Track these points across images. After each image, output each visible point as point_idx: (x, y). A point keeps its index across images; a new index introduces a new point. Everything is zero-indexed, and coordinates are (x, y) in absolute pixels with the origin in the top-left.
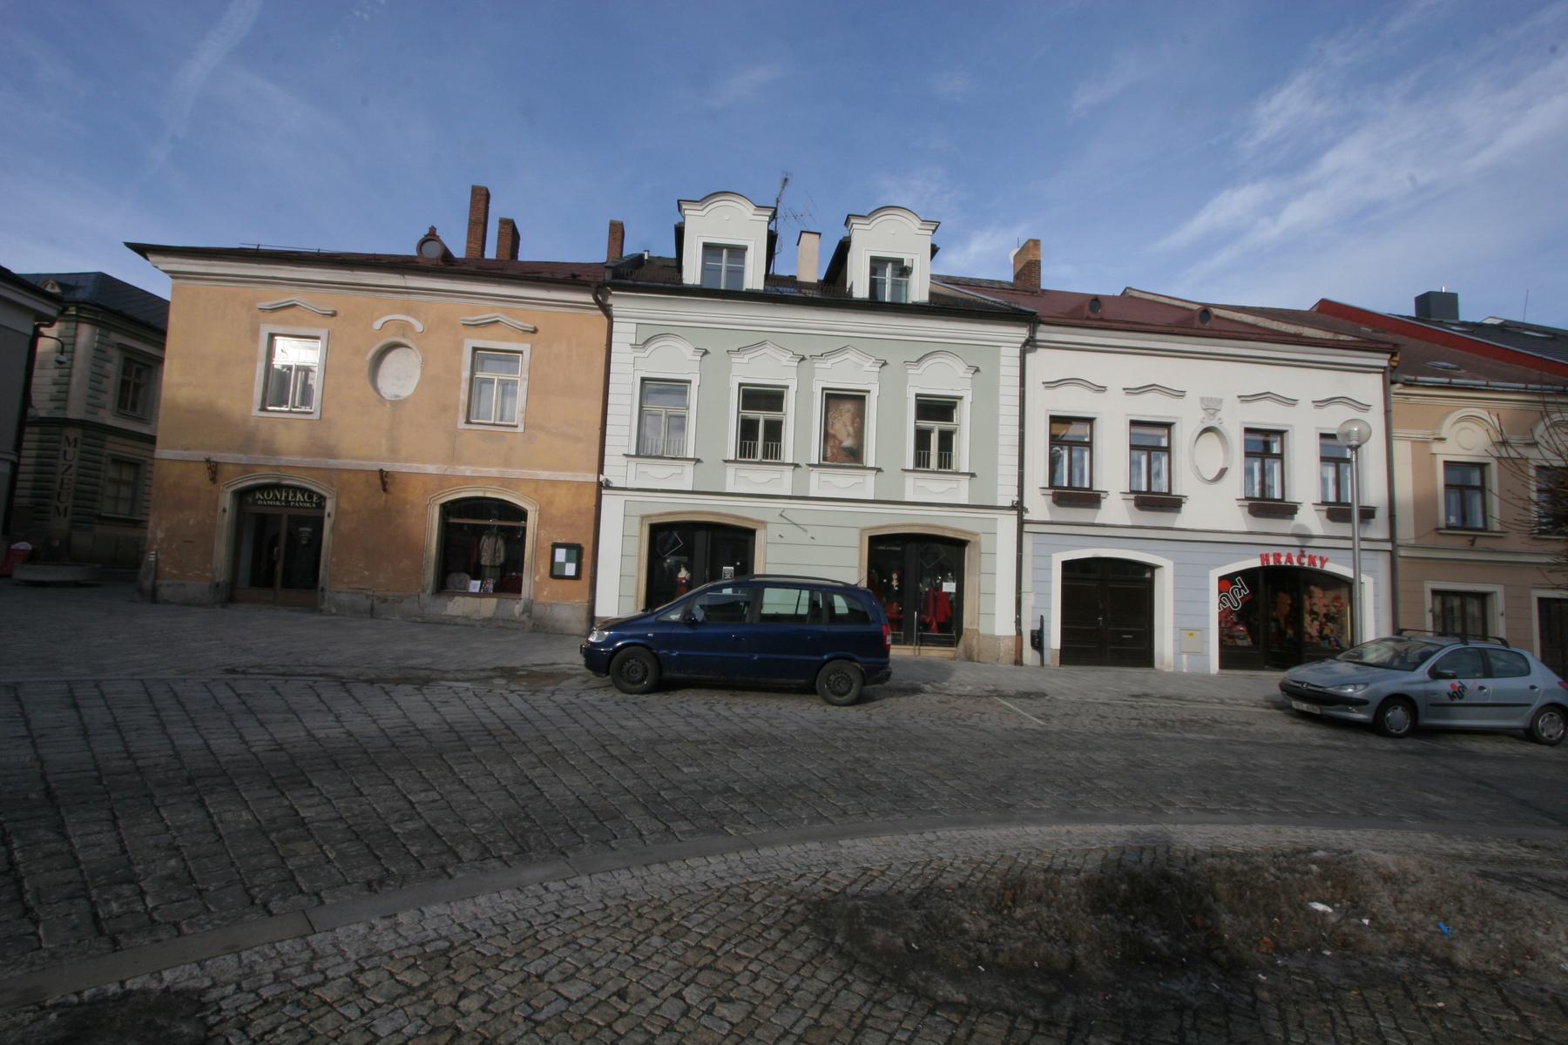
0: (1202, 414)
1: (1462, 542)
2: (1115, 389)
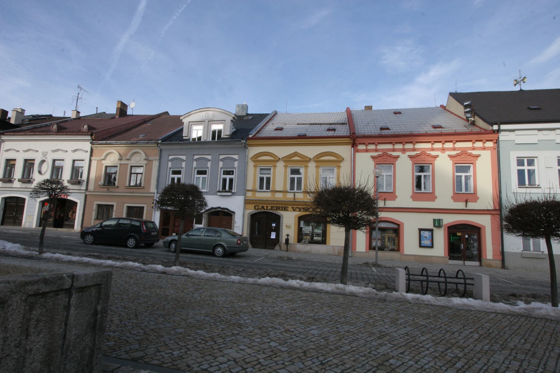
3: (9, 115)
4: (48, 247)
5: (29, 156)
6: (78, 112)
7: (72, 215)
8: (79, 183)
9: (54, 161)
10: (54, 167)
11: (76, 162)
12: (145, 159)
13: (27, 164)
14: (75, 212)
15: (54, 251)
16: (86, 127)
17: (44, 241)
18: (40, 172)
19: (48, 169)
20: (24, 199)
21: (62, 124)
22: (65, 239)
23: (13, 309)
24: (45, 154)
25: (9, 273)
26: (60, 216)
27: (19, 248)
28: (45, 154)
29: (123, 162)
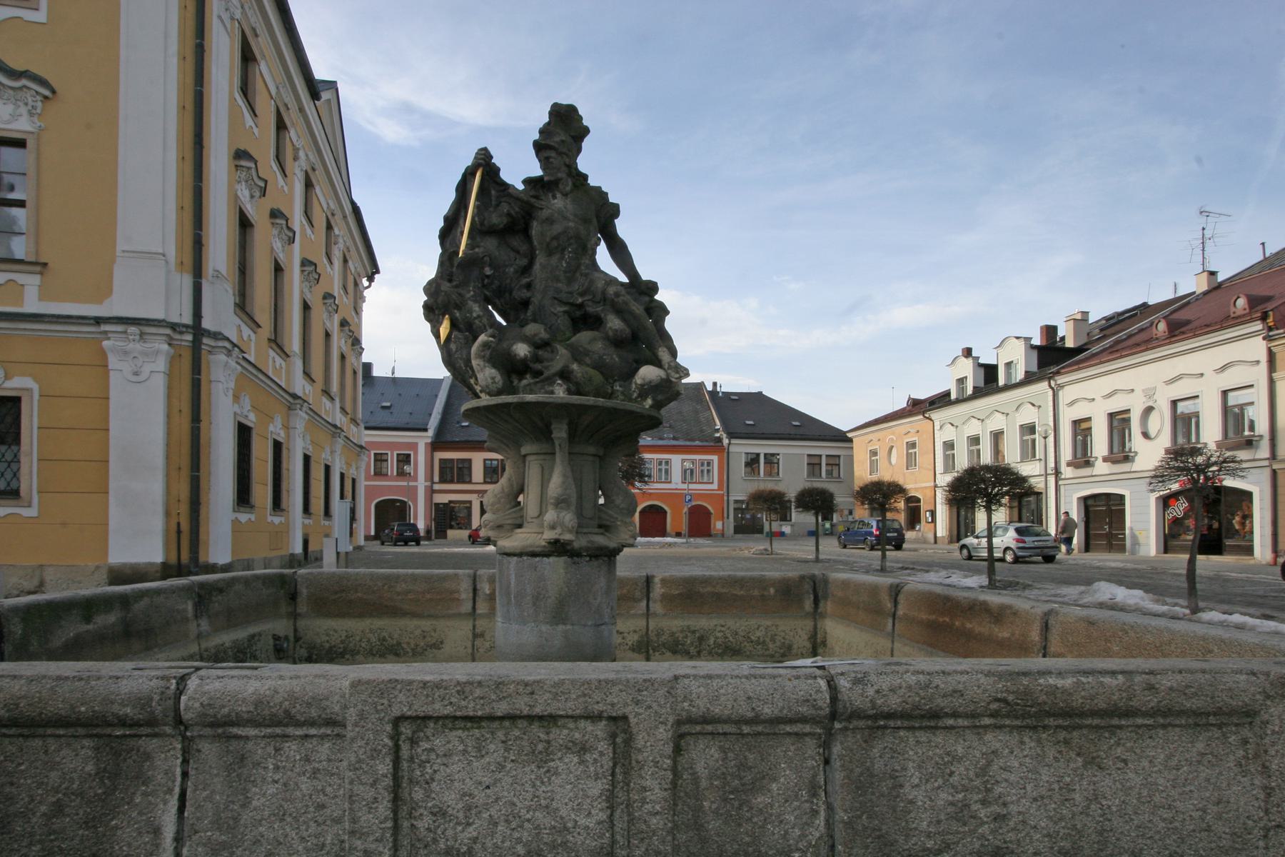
3: (1060, 333)
4: (1206, 599)
5: (1116, 405)
6: (1213, 274)
7: (1243, 524)
8: (1249, 443)
9: (1174, 403)
10: (1175, 418)
11: (1231, 395)
13: (1115, 423)
14: (1248, 516)
15: (1226, 607)
16: (1241, 302)
17: (1198, 586)
18: (1146, 435)
19: (1162, 425)
20: (1122, 497)
21: (1175, 316)
22: (1237, 580)
23: (1274, 732)
24: (1150, 393)
25: (1211, 652)
26: (1210, 527)
27: (1142, 598)
28: (1150, 393)
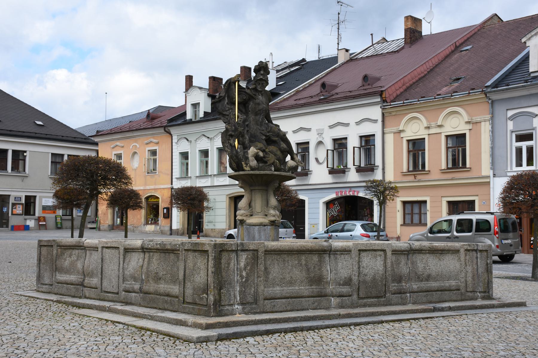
0: (317, 136)
1: (411, 178)
2: (353, 124)
12: (468, 123)
29: (432, 131)
